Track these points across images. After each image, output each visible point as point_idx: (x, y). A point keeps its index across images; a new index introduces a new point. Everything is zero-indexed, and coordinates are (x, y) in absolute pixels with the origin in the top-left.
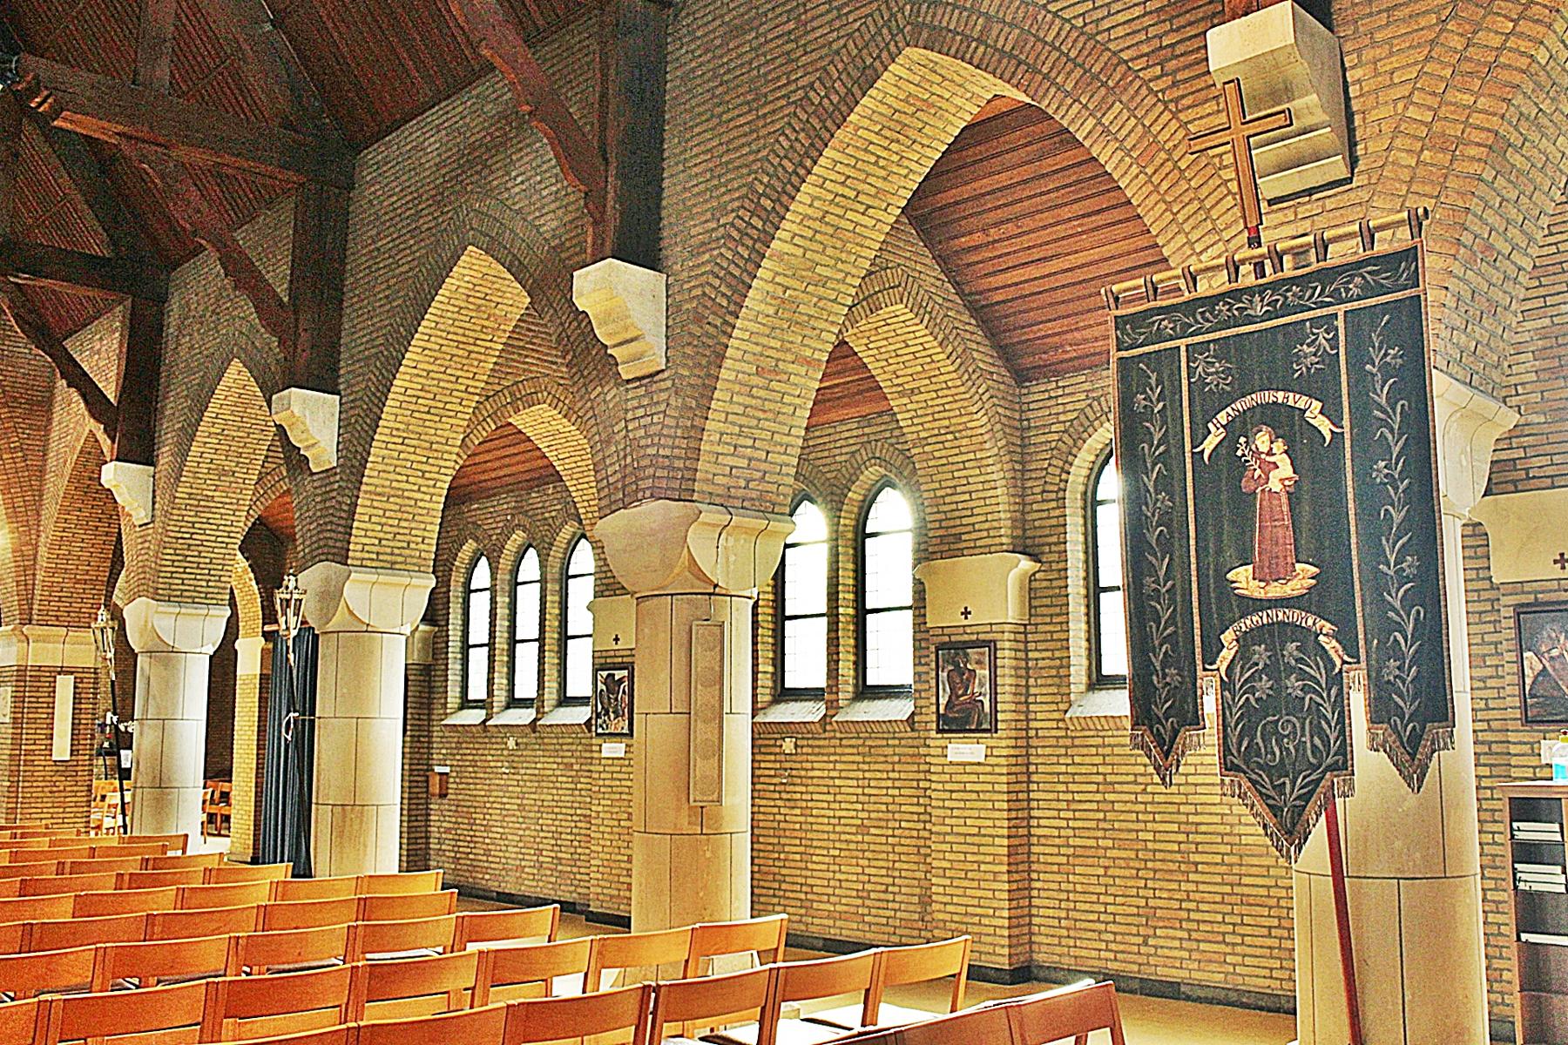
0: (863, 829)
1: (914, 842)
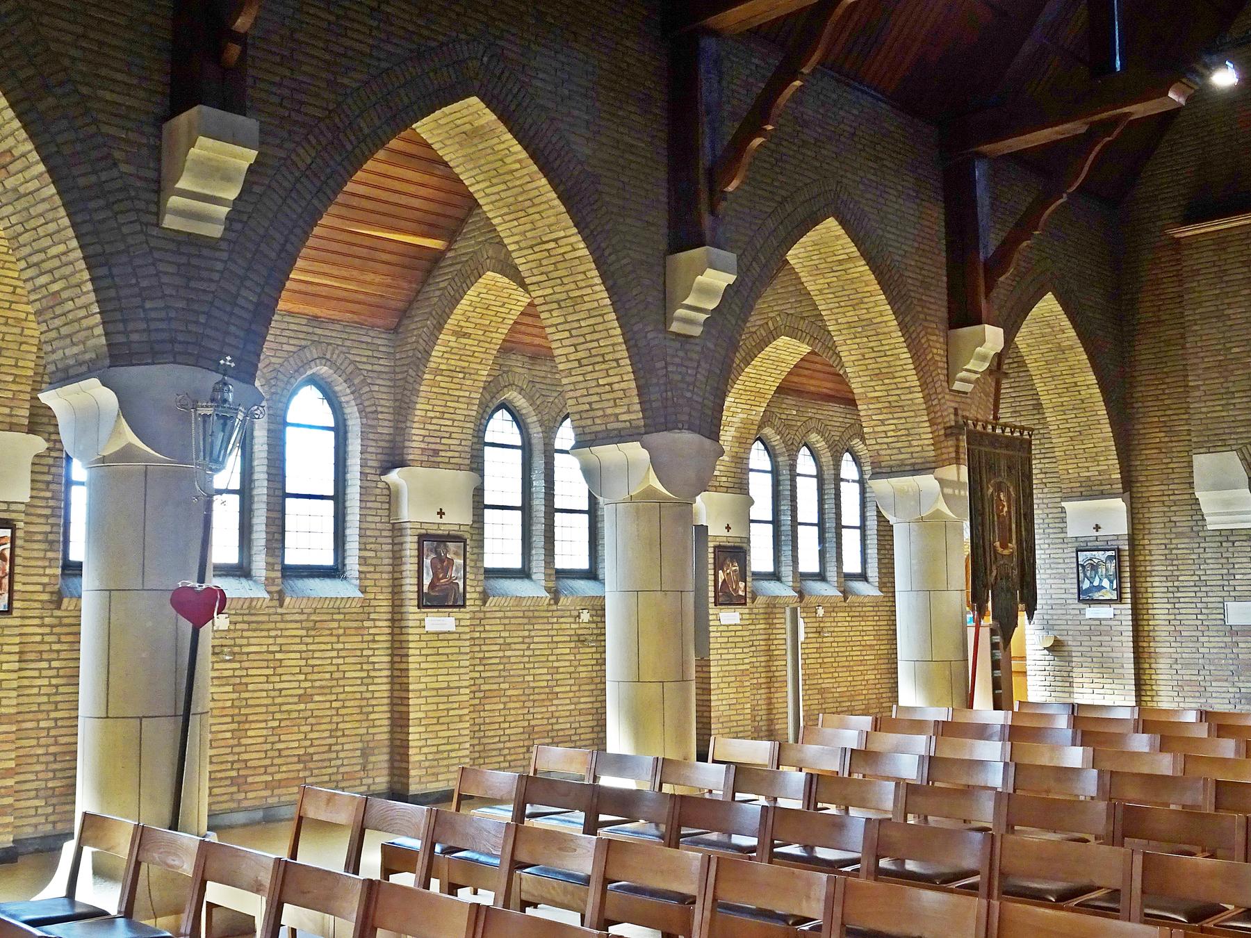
0: (304, 698)
1: (357, 703)
